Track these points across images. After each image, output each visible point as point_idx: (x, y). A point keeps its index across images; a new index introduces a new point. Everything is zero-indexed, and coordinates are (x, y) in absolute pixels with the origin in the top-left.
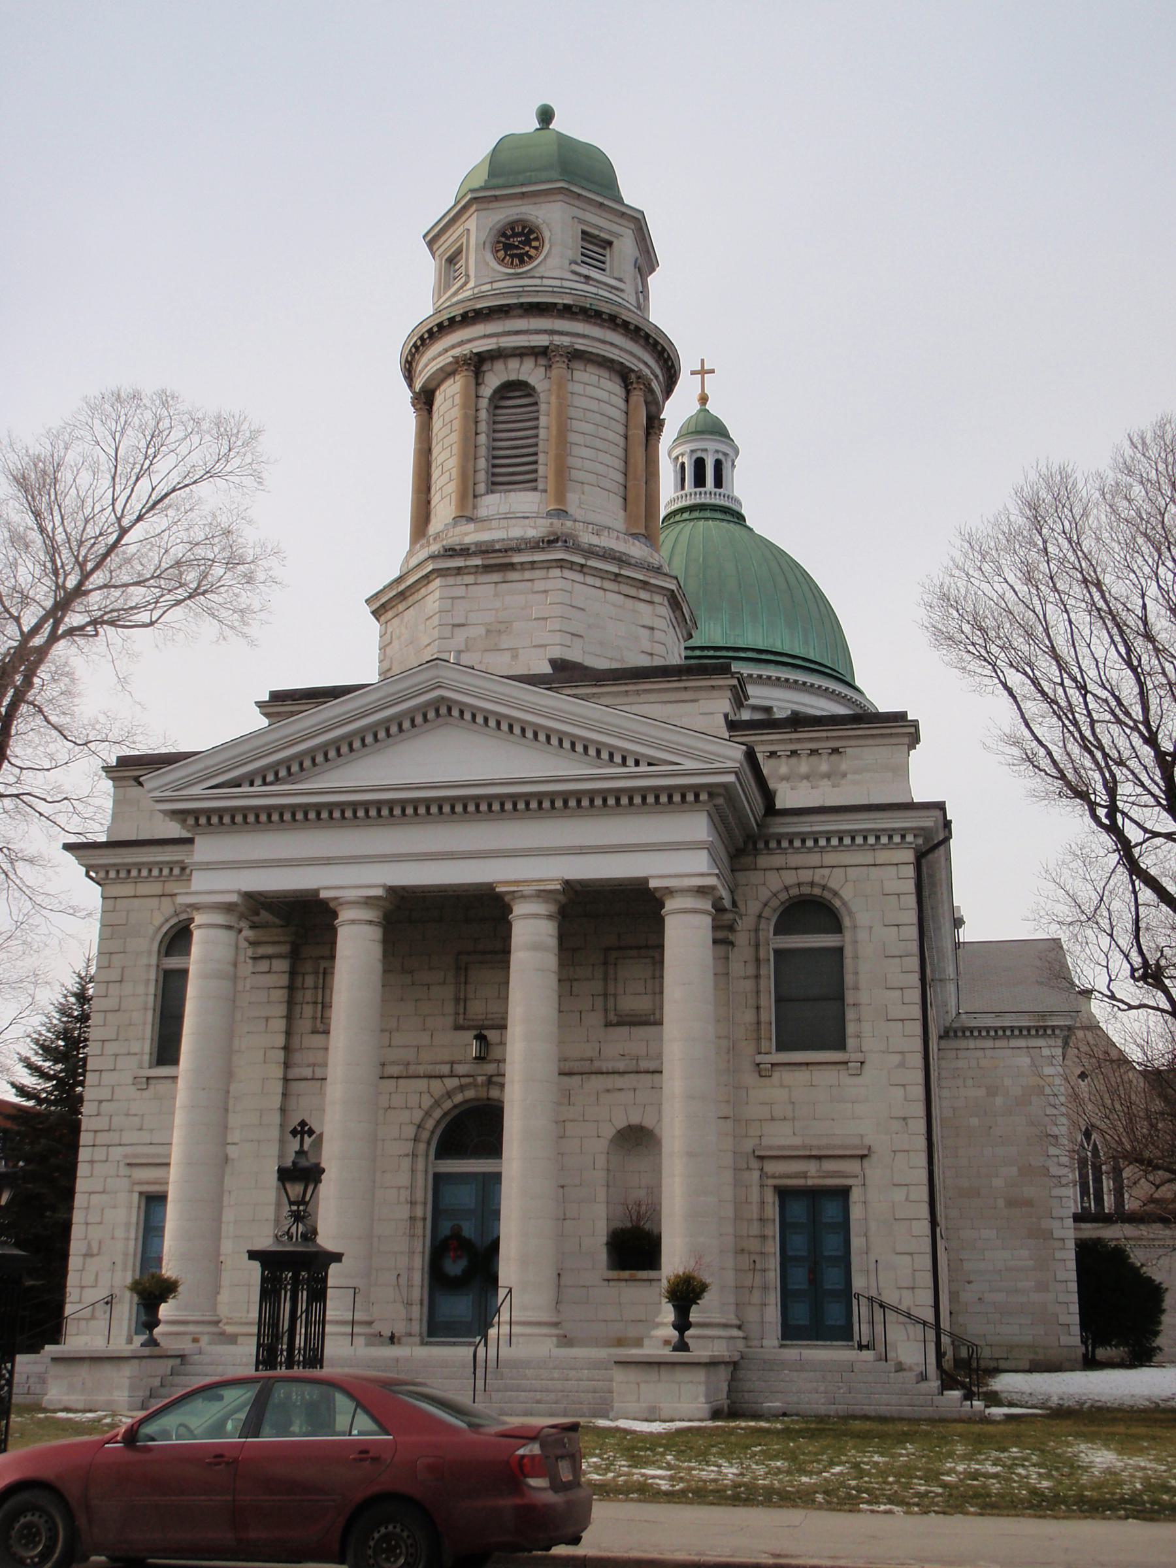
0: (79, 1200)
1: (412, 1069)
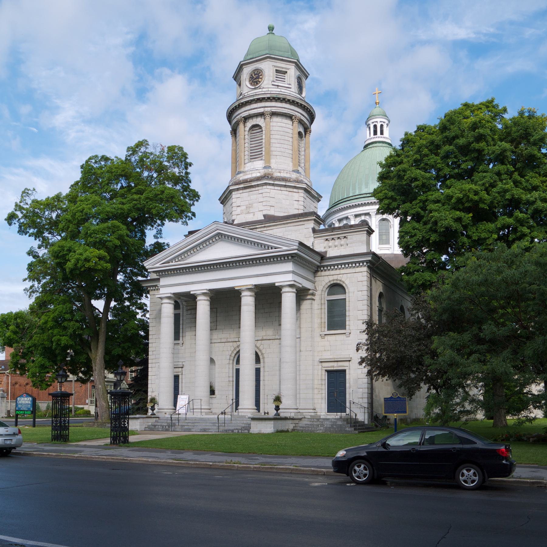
0: (149, 378)
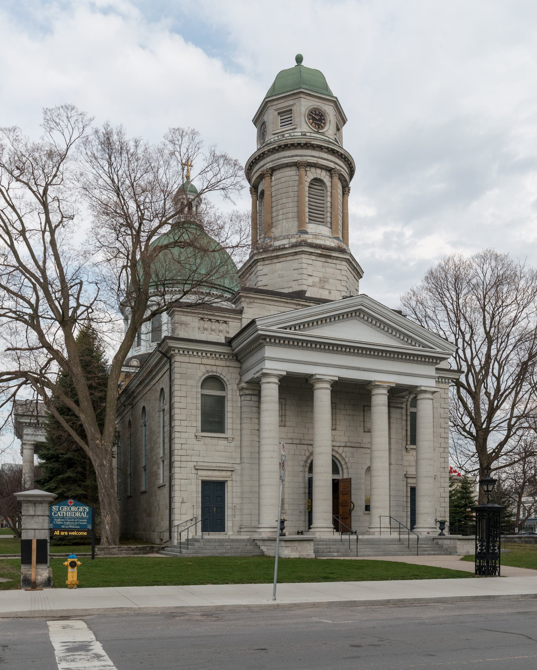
1: (303, 442)
